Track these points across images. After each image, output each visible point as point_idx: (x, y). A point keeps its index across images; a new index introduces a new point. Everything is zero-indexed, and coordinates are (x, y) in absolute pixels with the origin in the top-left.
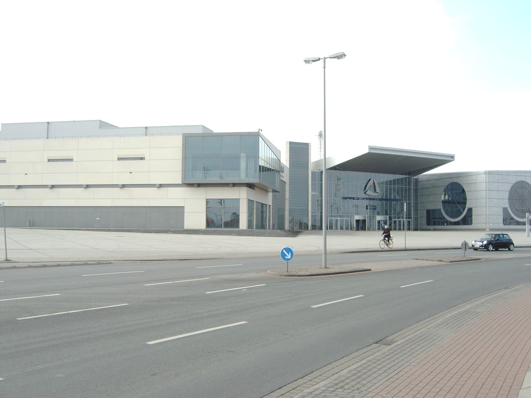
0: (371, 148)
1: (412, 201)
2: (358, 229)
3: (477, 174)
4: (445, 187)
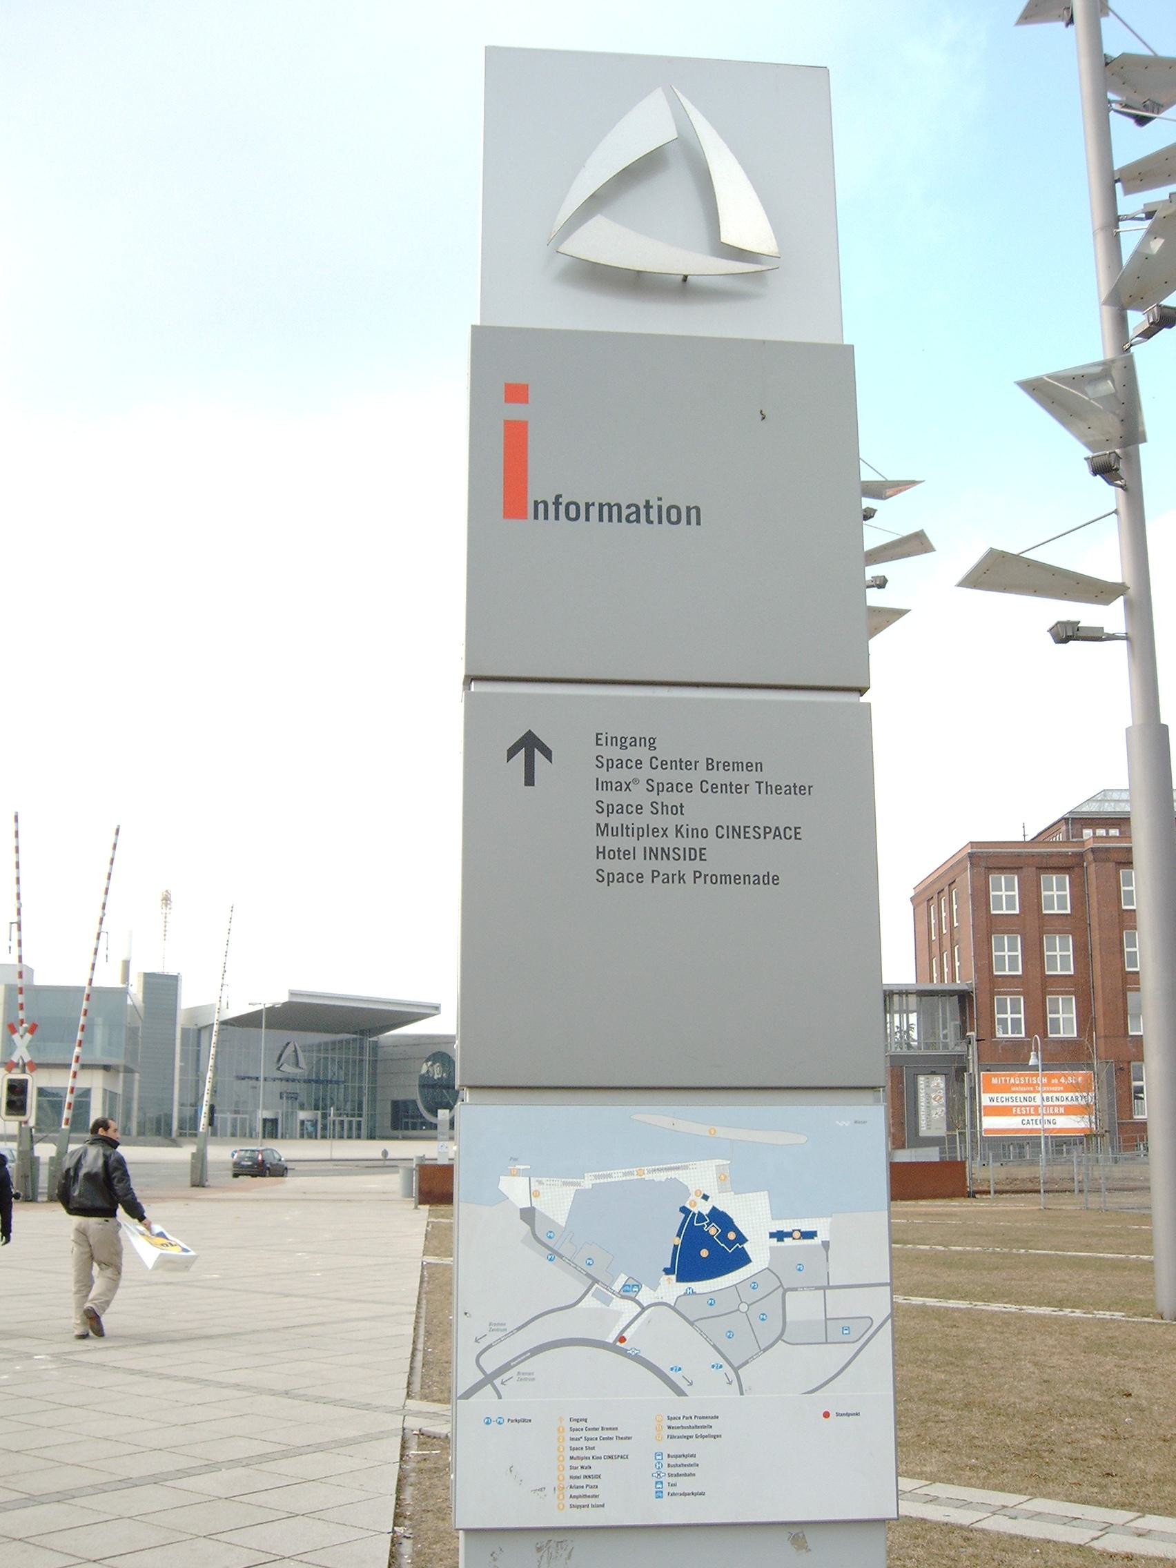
0: (292, 994)
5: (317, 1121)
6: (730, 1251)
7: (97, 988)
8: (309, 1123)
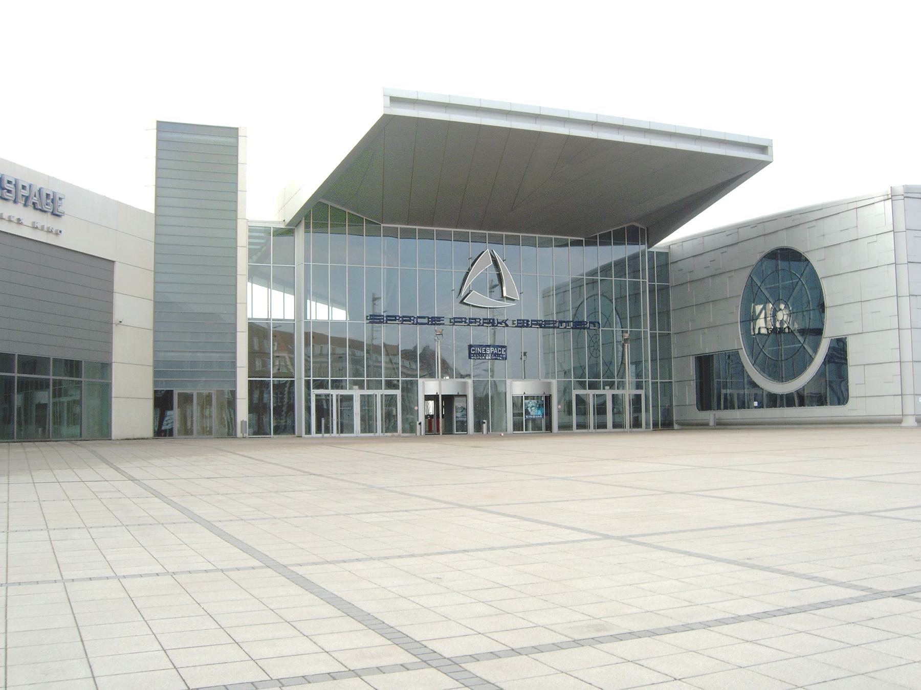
1: (646, 329)
2: (259, 429)
3: (860, 204)
4: (749, 271)
5: (548, 399)
6: (584, 239)
7: (847, 370)
8: (532, 403)
